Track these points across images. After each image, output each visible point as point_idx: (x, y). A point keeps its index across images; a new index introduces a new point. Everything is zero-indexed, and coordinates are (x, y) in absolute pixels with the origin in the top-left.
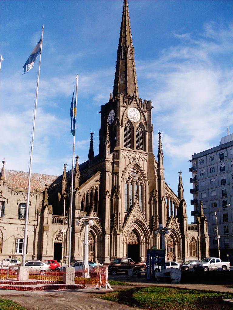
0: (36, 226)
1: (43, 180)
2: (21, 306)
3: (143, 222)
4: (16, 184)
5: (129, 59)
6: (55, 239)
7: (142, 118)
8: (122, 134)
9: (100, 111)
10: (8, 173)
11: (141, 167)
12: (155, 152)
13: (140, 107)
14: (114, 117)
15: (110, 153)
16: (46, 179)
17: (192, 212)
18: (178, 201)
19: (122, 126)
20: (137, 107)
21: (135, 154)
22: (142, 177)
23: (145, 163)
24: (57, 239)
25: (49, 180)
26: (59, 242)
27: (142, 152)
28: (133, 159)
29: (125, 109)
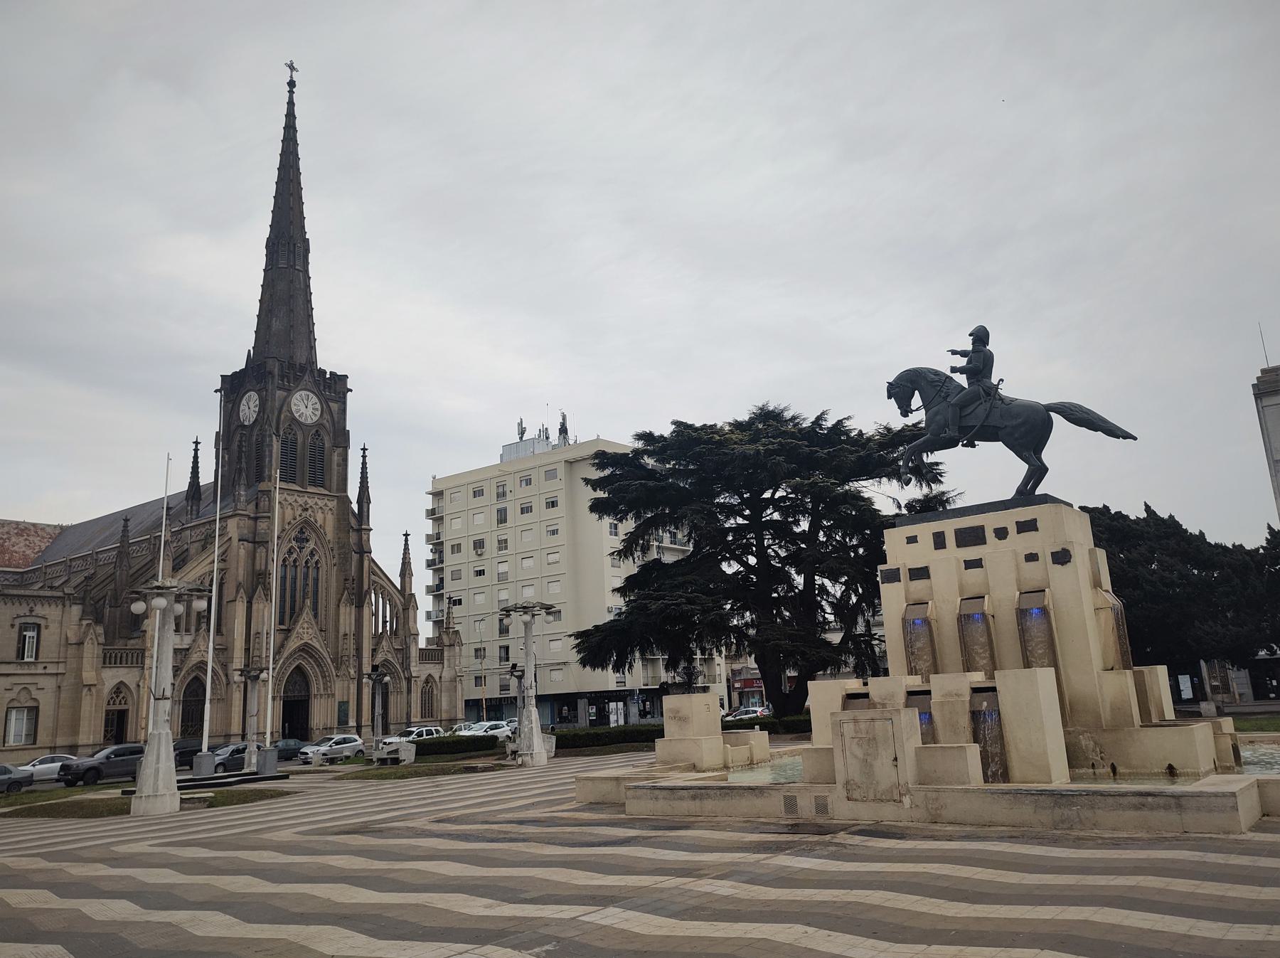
0: (256, 718)
1: (21, 539)
2: (1073, 641)
3: (321, 650)
5: (298, 270)
6: (109, 701)
7: (325, 415)
8: (277, 453)
11: (318, 526)
12: (353, 492)
13: (322, 388)
14: (257, 409)
18: (400, 600)
19: (278, 435)
20: (312, 390)
21: (306, 498)
22: (320, 545)
23: (330, 517)
24: (112, 703)
25: (39, 538)
26: (118, 707)
27: (324, 493)
28: (300, 509)
29: (285, 394)
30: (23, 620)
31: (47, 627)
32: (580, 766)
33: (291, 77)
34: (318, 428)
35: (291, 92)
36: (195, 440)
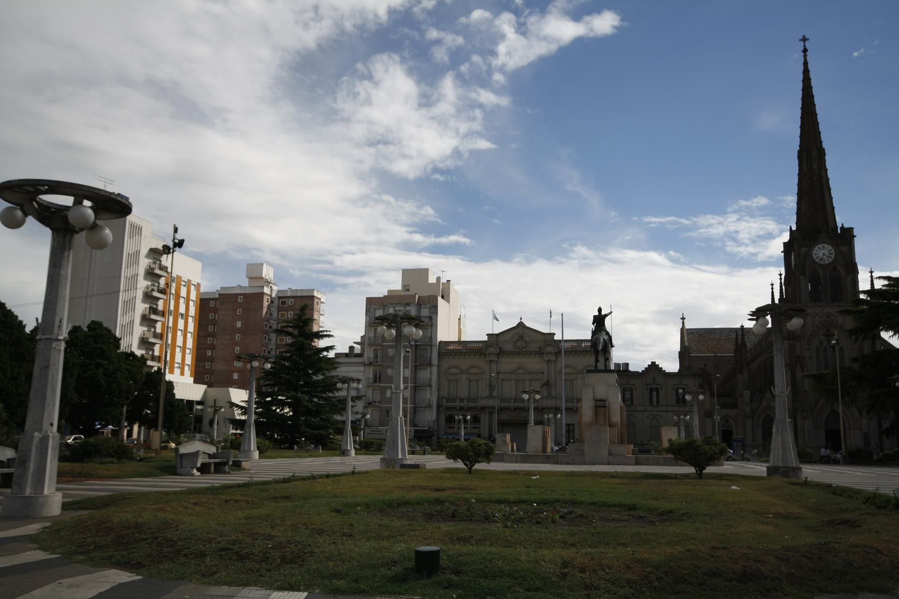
4: (702, 348)
9: (783, 250)
10: (690, 333)
15: (355, 402)
16: (749, 335)
17: (655, 362)
24: (724, 426)
30: (651, 386)
31: (635, 389)
32: (134, 244)
33: (805, 46)
34: (833, 266)
35: (805, 56)
36: (682, 317)
